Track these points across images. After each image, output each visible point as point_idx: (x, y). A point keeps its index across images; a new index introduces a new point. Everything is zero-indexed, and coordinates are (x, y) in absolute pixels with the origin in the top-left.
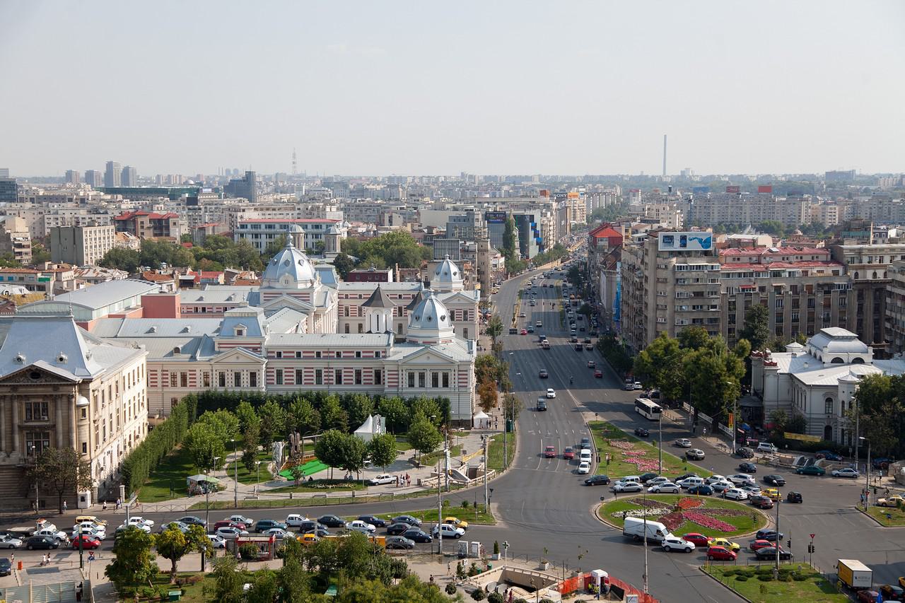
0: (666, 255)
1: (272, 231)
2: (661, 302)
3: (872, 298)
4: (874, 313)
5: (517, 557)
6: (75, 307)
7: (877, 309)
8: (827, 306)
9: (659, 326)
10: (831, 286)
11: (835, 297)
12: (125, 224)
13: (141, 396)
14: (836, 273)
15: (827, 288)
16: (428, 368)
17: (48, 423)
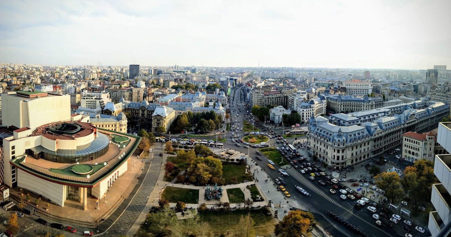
4: (437, 134)
5: (267, 173)
7: (287, 100)
11: (281, 98)
12: (176, 80)
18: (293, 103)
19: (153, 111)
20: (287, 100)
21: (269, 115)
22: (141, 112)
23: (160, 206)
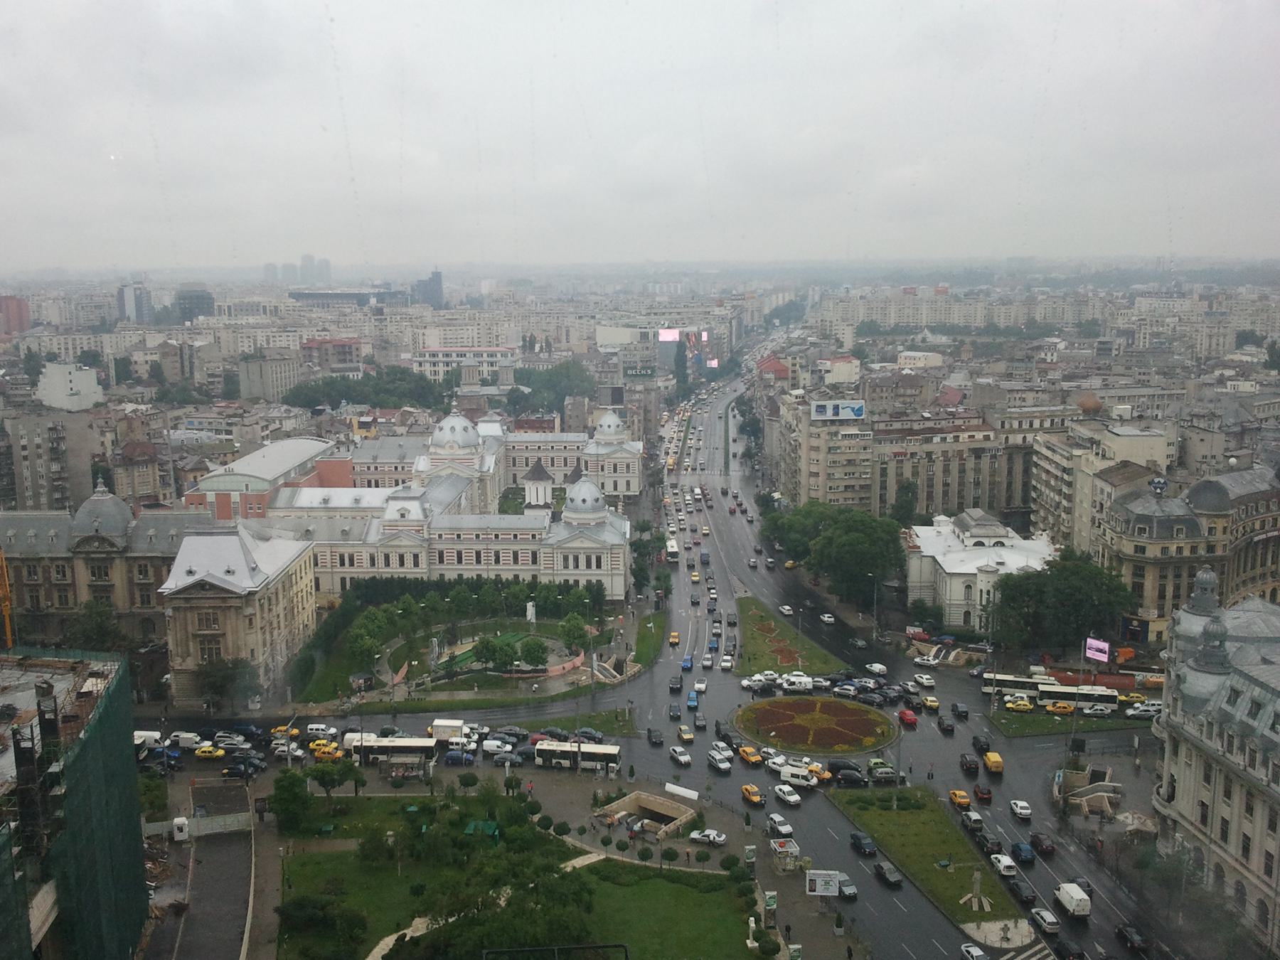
0: (820, 424)
1: (449, 359)
2: (814, 469)
3: (1021, 462)
6: (252, 479)
7: (1027, 471)
8: (977, 470)
9: (811, 492)
10: (983, 450)
11: (985, 461)
13: (309, 586)
14: (987, 438)
15: (978, 453)
16: (582, 551)
17: (219, 632)
18: (1069, 498)
19: (168, 561)
20: (1027, 471)
21: (904, 576)
22: (83, 575)
23: (175, 581)
